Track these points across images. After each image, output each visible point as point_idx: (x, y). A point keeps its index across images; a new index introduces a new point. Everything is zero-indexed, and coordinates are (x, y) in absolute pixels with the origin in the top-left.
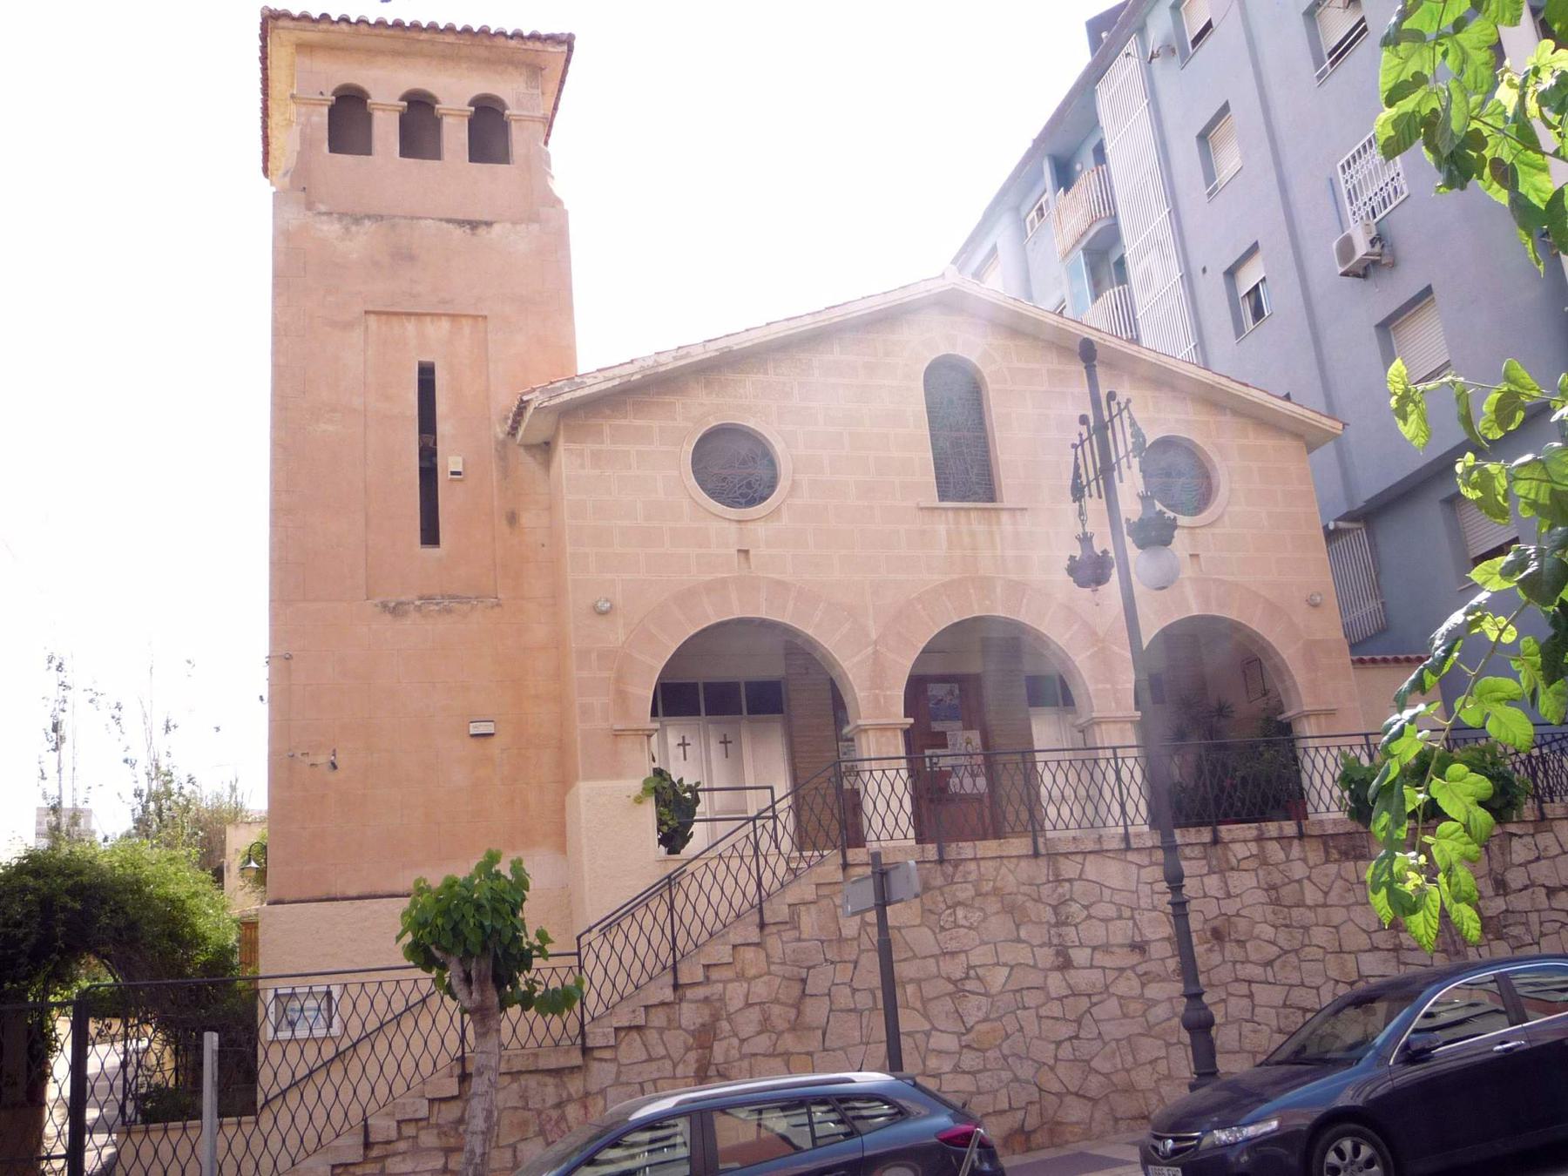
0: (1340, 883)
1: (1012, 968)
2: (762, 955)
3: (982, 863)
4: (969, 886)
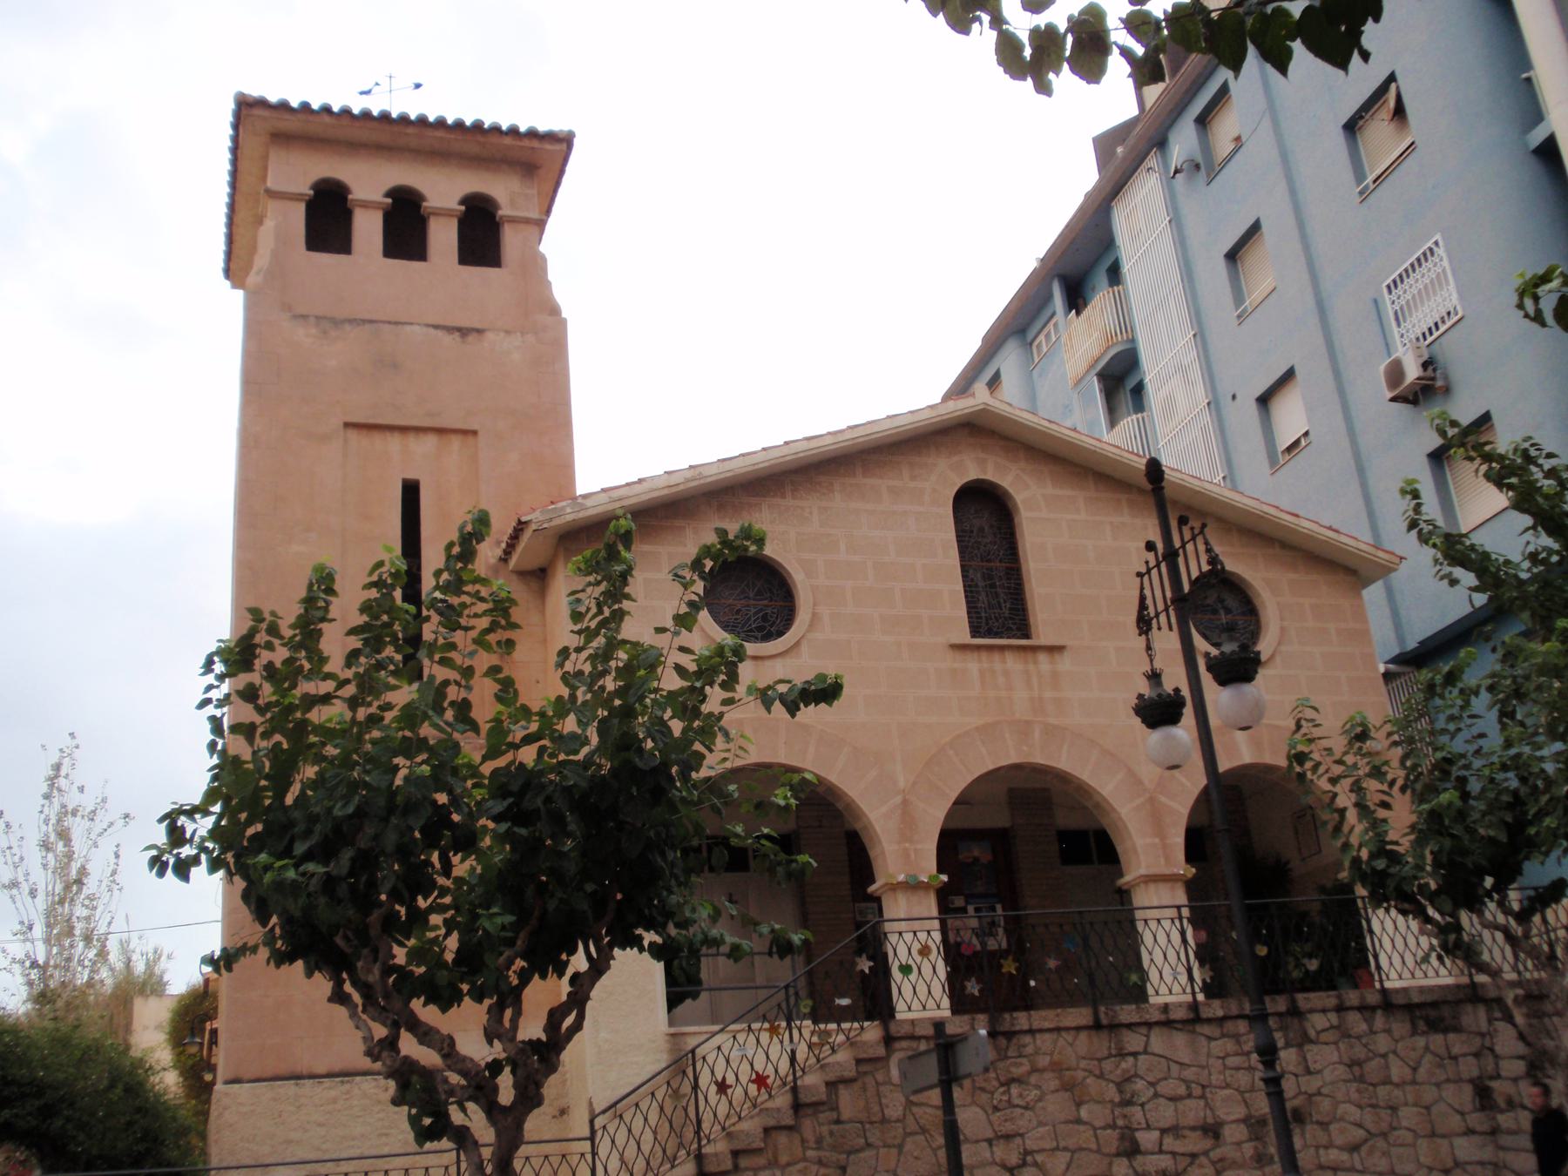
0: (1429, 1057)
1: (1073, 1152)
2: (797, 1141)
3: (1038, 1036)
4: (1024, 1061)
